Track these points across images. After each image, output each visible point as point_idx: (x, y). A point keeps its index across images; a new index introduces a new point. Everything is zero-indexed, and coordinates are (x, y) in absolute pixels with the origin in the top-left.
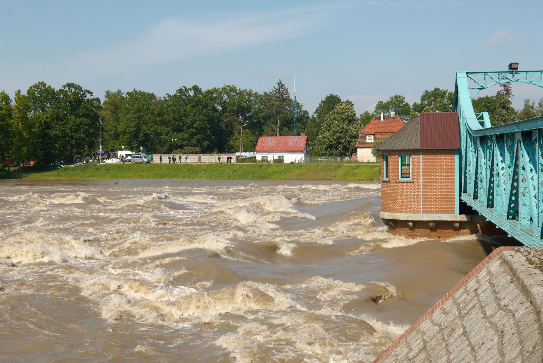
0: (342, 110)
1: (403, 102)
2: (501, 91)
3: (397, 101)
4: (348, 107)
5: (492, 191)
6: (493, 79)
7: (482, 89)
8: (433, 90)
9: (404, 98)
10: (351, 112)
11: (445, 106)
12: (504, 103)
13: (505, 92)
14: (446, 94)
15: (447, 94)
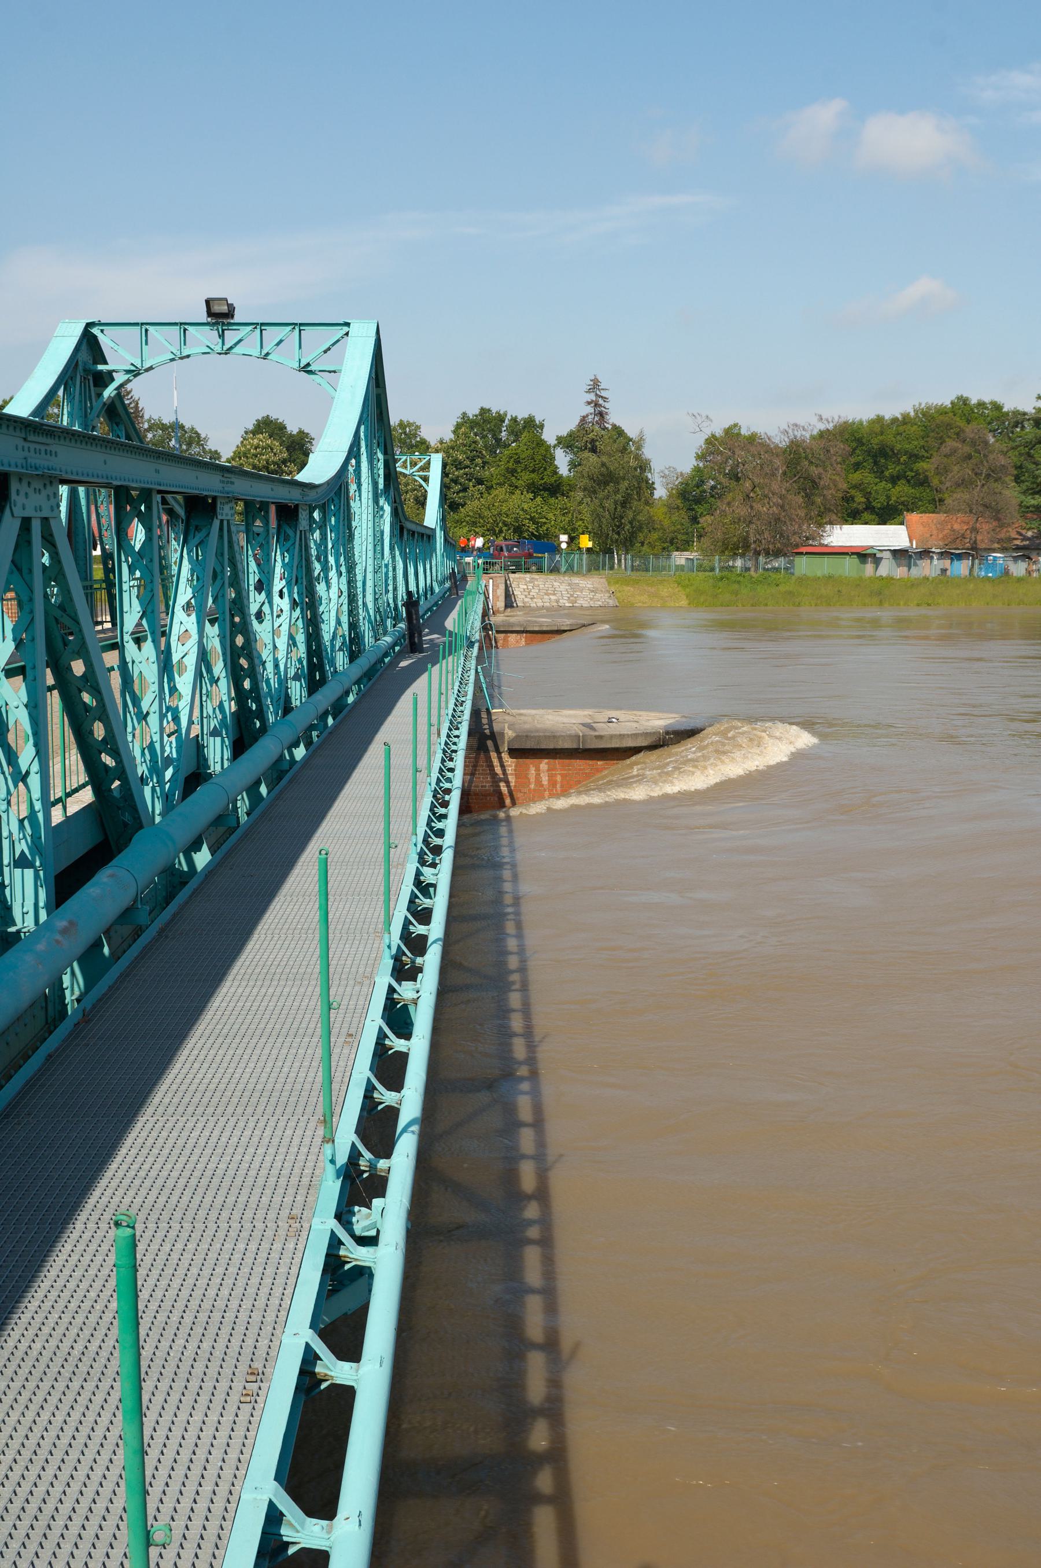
0: (256, 448)
1: (415, 436)
2: (587, 416)
3: (405, 433)
4: (269, 442)
5: (240, 640)
6: (281, 341)
7: (208, 353)
8: (477, 412)
9: (418, 427)
10: (275, 454)
11: (473, 445)
12: (593, 441)
13: (597, 419)
14: (504, 422)
15: (507, 422)
